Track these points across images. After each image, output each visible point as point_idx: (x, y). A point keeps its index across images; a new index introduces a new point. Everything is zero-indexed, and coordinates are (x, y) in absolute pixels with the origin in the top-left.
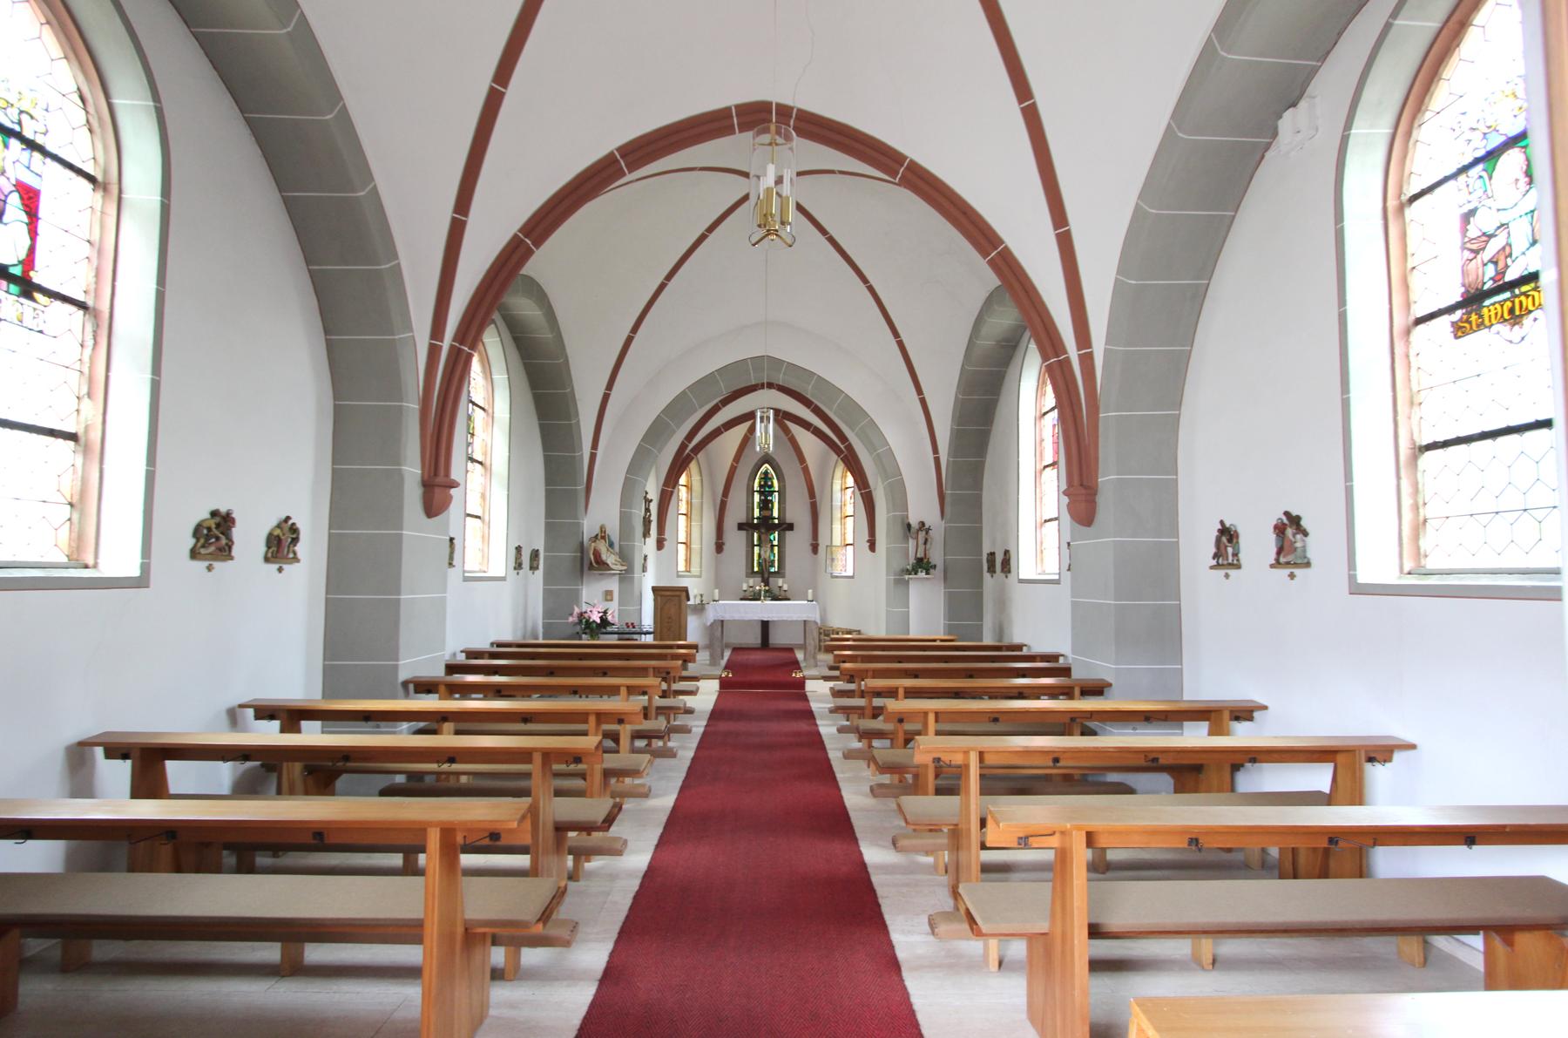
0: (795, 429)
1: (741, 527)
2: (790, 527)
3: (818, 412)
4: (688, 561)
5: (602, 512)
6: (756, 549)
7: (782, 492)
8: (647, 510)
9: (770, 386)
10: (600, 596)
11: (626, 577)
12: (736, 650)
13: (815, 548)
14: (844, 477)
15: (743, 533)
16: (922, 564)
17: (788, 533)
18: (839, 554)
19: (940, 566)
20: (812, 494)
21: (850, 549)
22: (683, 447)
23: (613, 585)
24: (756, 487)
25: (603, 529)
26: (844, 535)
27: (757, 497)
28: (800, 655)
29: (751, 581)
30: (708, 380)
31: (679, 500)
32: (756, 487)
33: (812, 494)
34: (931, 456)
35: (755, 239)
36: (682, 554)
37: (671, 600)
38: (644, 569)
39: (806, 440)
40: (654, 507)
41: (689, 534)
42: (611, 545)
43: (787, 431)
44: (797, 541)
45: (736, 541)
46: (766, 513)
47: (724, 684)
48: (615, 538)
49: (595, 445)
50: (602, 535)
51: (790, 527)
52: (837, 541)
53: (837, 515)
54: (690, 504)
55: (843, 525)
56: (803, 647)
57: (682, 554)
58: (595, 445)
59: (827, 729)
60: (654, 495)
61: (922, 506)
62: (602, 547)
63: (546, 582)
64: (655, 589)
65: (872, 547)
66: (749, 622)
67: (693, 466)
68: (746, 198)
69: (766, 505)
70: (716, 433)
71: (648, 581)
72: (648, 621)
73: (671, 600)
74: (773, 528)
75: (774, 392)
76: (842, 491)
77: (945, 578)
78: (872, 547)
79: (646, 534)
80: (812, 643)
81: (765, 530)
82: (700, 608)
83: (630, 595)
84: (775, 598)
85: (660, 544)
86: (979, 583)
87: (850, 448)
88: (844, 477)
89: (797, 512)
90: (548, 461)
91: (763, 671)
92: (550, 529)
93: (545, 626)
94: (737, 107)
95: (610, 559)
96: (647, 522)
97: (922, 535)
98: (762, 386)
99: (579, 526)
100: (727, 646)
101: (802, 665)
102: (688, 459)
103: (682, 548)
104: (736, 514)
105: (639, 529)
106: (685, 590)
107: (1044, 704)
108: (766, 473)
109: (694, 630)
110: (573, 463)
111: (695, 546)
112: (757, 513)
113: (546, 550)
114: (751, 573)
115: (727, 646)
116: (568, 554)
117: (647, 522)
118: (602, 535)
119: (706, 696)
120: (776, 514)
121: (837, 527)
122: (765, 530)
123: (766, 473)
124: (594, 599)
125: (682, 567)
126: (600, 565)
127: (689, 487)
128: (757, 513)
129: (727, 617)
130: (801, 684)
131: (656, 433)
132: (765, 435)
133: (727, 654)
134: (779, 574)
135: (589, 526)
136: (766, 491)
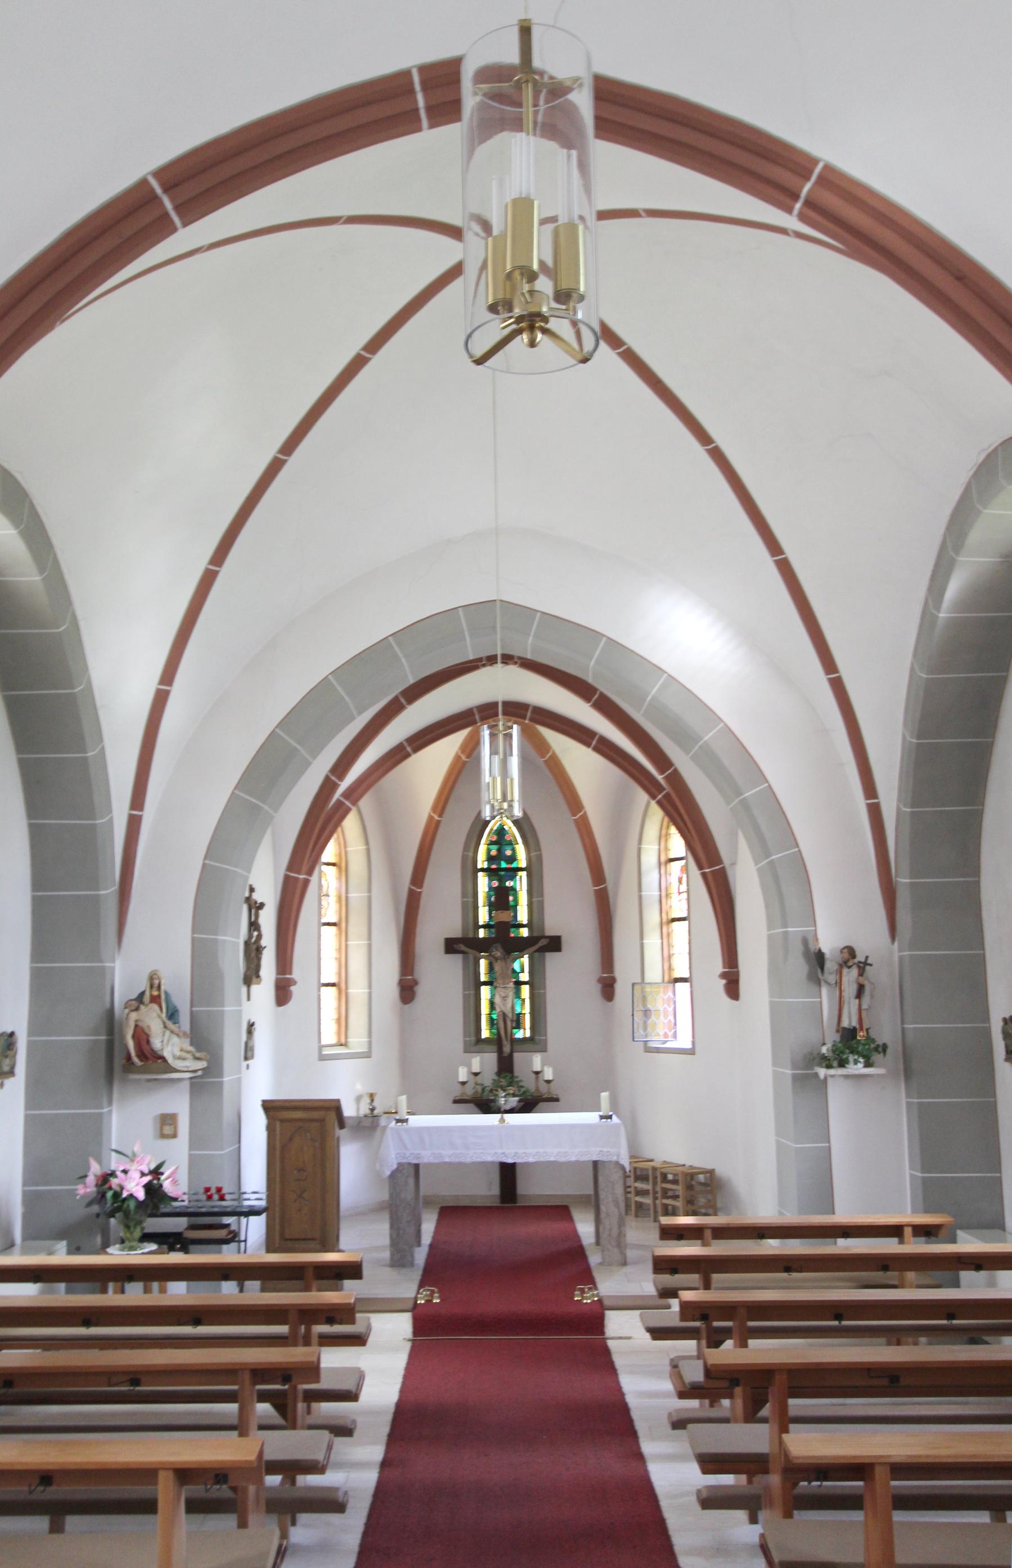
0: (558, 741)
1: (451, 946)
2: (555, 944)
3: (606, 707)
4: (343, 1022)
5: (154, 946)
6: (485, 992)
7: (534, 871)
8: (254, 925)
9: (507, 659)
10: (148, 1126)
11: (207, 1083)
12: (451, 1212)
13: (608, 988)
14: (663, 837)
15: (457, 960)
16: (852, 1044)
17: (551, 958)
18: (659, 1001)
19: (895, 1048)
20: (598, 874)
21: (683, 988)
22: (328, 787)
23: (178, 1103)
24: (482, 862)
25: (154, 982)
26: (667, 959)
27: (483, 882)
28: (585, 1228)
29: (476, 1063)
30: (377, 654)
31: (321, 895)
32: (482, 862)
33: (598, 874)
34: (861, 803)
35: (481, 346)
36: (329, 1025)
37: (304, 1130)
38: (248, 1053)
39: (580, 763)
40: (268, 920)
41: (343, 965)
42: (173, 1015)
43: (542, 747)
44: (570, 972)
45: (441, 975)
46: (504, 916)
47: (425, 1325)
48: (182, 1002)
49: (138, 799)
50: (153, 994)
51: (555, 944)
52: (654, 973)
53: (652, 917)
54: (344, 901)
55: (666, 938)
56: (593, 1202)
57: (329, 1025)
58: (138, 799)
59: (674, 1475)
60: (268, 894)
61: (844, 914)
62: (153, 1019)
63: (32, 1099)
64: (269, 1107)
65: (732, 987)
66: (484, 1164)
67: (350, 824)
68: (455, 271)
69: (501, 899)
70: (397, 755)
71: (256, 1084)
72: (254, 1180)
73: (304, 1130)
74: (520, 946)
75: (514, 670)
76: (658, 865)
77: (908, 1073)
78: (732, 987)
79: (251, 976)
80: (613, 1193)
81: (499, 947)
82: (369, 1125)
83: (213, 1128)
84: (528, 1106)
85: (283, 994)
86: (986, 1082)
87: (676, 779)
88: (663, 837)
89: (569, 914)
90: (37, 836)
91: (506, 1272)
92: (42, 983)
93: (30, 1200)
94: (423, 69)
95: (170, 1046)
96: (253, 951)
97: (850, 976)
98: (491, 660)
99: (101, 976)
100: (428, 1202)
101: (594, 1259)
102: (340, 812)
103: (329, 995)
104: (441, 920)
105: (234, 962)
106: (335, 1107)
107: (682, 811)
108: (501, 832)
109: (355, 1172)
110: (89, 841)
111: (358, 990)
112: (483, 916)
113: (32, 1031)
114: (475, 1043)
115: (428, 1202)
116: (80, 1037)
117: (253, 951)
118: (153, 994)
119: (379, 1365)
120: (523, 916)
121: (653, 942)
122: (499, 947)
123: (501, 832)
124: (139, 1142)
125: (329, 1035)
126: (149, 1060)
127: (341, 866)
128: (483, 916)
129: (426, 1156)
130: (593, 1322)
131: (267, 770)
132: (502, 777)
133: (428, 1227)
134: (535, 1042)
135: (124, 975)
136: (501, 870)
